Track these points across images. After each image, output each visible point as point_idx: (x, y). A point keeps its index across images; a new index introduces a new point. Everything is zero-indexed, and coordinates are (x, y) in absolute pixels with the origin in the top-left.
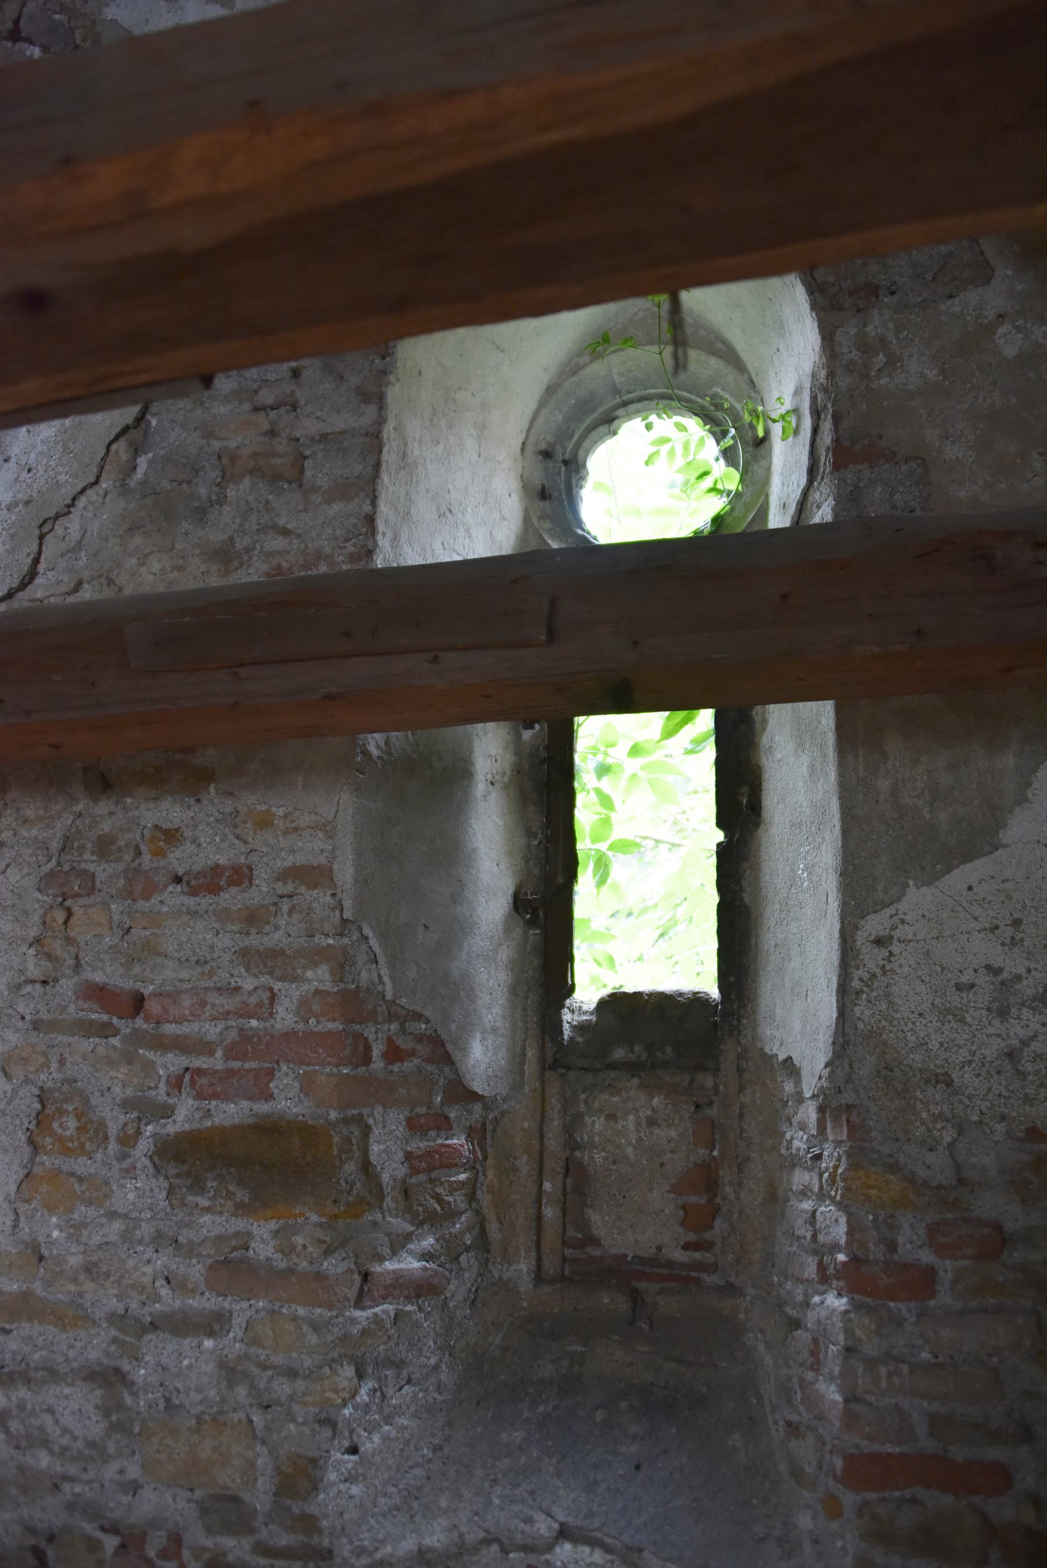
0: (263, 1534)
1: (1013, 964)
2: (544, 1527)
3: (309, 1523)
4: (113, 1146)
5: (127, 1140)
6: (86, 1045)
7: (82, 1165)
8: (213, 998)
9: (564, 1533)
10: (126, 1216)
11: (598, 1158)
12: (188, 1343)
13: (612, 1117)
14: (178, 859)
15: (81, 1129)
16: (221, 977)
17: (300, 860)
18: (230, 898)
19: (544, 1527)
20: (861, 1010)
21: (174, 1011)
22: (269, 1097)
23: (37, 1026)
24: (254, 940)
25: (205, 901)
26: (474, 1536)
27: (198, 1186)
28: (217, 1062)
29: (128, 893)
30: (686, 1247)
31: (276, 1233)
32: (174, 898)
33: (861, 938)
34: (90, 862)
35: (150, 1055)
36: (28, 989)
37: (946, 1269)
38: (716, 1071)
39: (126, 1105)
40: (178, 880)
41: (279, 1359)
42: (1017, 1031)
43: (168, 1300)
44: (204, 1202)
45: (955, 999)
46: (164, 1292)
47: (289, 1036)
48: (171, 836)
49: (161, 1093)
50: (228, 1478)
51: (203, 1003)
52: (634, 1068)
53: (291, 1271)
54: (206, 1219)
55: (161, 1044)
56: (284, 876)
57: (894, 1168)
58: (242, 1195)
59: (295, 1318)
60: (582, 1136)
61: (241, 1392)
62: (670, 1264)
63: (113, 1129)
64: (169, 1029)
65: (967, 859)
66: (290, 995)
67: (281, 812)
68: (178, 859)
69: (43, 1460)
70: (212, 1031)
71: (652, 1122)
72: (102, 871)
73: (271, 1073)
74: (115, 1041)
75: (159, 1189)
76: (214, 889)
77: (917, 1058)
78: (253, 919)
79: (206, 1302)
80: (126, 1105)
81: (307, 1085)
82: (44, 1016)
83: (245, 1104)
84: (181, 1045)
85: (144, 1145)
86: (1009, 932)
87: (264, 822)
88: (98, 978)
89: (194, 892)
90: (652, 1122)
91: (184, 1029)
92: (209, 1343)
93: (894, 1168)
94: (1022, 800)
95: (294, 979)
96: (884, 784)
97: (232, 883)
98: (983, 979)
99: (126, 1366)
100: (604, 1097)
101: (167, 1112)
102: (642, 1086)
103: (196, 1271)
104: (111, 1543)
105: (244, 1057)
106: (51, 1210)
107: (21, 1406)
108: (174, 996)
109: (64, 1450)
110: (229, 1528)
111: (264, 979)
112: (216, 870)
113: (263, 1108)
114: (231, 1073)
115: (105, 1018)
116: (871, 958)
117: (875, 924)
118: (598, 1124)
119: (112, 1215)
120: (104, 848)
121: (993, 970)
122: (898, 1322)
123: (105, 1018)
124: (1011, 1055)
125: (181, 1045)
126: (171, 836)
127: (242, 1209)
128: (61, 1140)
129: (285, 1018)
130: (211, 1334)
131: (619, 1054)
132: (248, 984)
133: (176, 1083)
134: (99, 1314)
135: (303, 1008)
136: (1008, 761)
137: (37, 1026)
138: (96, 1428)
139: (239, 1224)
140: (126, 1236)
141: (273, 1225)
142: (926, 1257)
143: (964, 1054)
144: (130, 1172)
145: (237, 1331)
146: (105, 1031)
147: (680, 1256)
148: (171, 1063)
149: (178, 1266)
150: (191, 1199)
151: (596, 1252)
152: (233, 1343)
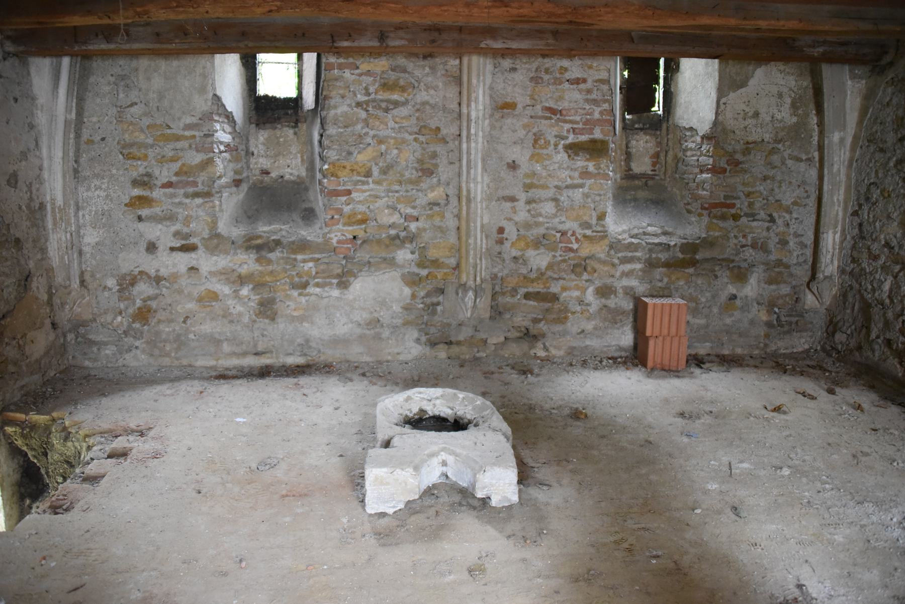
0: (595, 229)
1: (747, 110)
2: (644, 224)
3: (603, 226)
4: (552, 147)
5: (556, 145)
6: (543, 121)
7: (545, 152)
8: (579, 110)
9: (649, 225)
10: (558, 163)
11: (634, 150)
12: (576, 190)
13: (637, 141)
14: (567, 75)
15: (545, 143)
16: (580, 106)
17: (600, 77)
18: (582, 86)
19: (644, 224)
20: (720, 117)
21: (570, 114)
22: (593, 134)
23: (531, 117)
24: (589, 97)
25: (575, 86)
26: (632, 227)
27: (577, 154)
28: (581, 126)
29: (554, 83)
30: (652, 171)
31: (594, 165)
32: (567, 85)
33: (721, 102)
34: (543, 75)
35: (562, 124)
36: (528, 108)
37: (729, 168)
38: (661, 130)
39: (556, 136)
40: (568, 81)
41: (596, 193)
42: (747, 123)
43: (569, 181)
44: (579, 158)
45: (736, 116)
46: (569, 180)
47: (598, 120)
48: (566, 70)
49: (565, 134)
50: (586, 218)
51: (577, 112)
52: (641, 129)
53: (599, 173)
54: (579, 162)
55: (566, 122)
56: (596, 81)
57: (723, 149)
58: (588, 157)
59: (601, 183)
60: (630, 145)
61: (589, 200)
62: (648, 175)
63: (552, 142)
64: (567, 118)
65: (742, 88)
66: (597, 110)
67: (595, 65)
68: (567, 75)
69: (541, 219)
70: (578, 118)
71: (646, 142)
72: (546, 77)
73: (593, 129)
74: (553, 121)
75: (566, 155)
76: (578, 84)
77: (729, 128)
78: (589, 91)
79: (580, 181)
80: (556, 136)
81: (602, 131)
82: (533, 114)
83: (587, 136)
84: (571, 122)
85: (560, 147)
86: (747, 103)
87: (590, 67)
88: (547, 105)
89: (572, 84)
90: (646, 142)
91: (571, 118)
92: (581, 190)
93: (723, 149)
94: (752, 76)
95: (599, 106)
96: (728, 70)
97: (583, 82)
98: (742, 112)
99: (559, 197)
100: (635, 136)
101: (567, 138)
102: (644, 133)
103: (576, 174)
104: (558, 235)
105: (587, 125)
106: (537, 162)
107: (534, 208)
108: (569, 110)
109: (546, 216)
110: (587, 228)
111: (592, 106)
112: (578, 79)
113: (591, 136)
114: (584, 129)
115: (549, 115)
116: (722, 107)
117: (723, 100)
118: (634, 143)
119: (555, 163)
120: (547, 71)
121: (744, 111)
122: (720, 178)
123: (549, 115)
124: (746, 128)
125: (571, 122)
126: (566, 70)
127: (587, 160)
128: (540, 145)
129: (597, 115)
130: (582, 188)
131: (636, 126)
132: (588, 107)
133: (568, 131)
134: (551, 186)
135: (601, 113)
136: (751, 68)
137: (531, 117)
138: (554, 211)
139: (586, 163)
140: (559, 168)
141: (594, 163)
142: (726, 166)
143: (737, 127)
144: (559, 152)
145: (587, 187)
146: (550, 118)
147: (650, 173)
148: (567, 126)
149: (572, 174)
150: (576, 158)
151: (631, 172)
152: (586, 190)
